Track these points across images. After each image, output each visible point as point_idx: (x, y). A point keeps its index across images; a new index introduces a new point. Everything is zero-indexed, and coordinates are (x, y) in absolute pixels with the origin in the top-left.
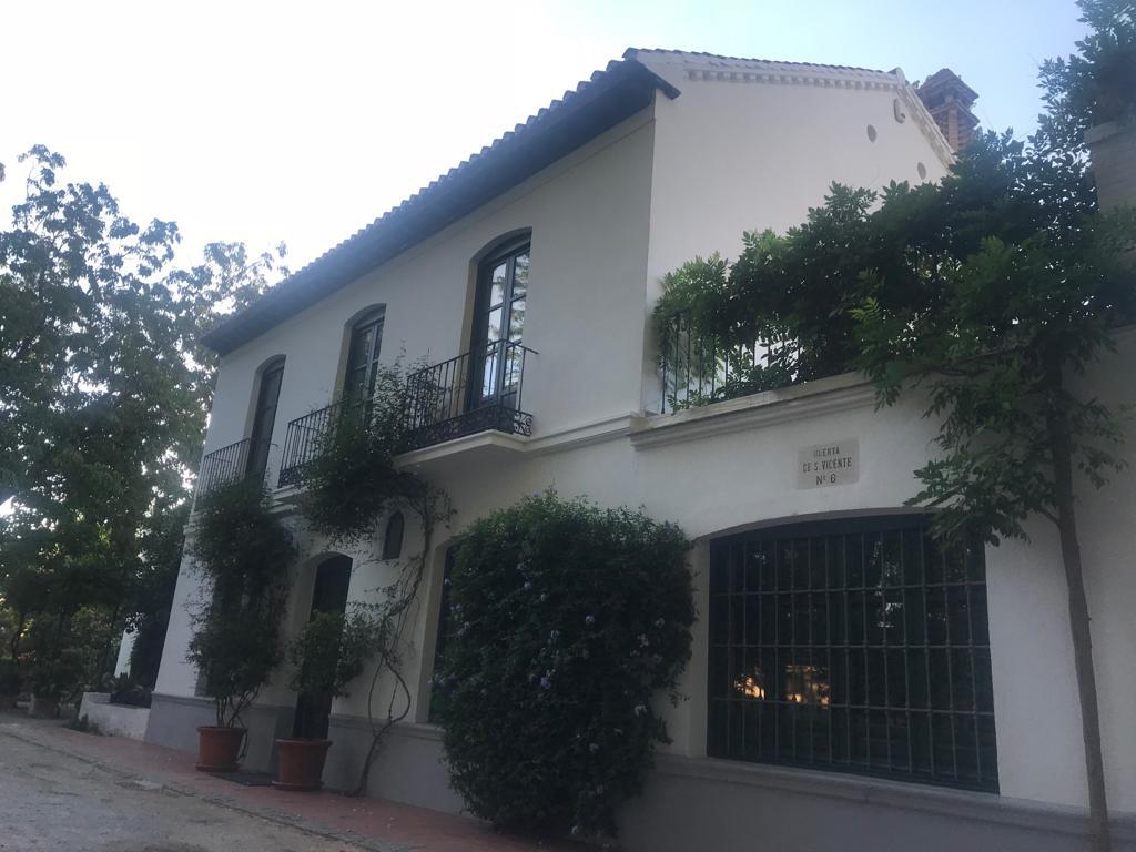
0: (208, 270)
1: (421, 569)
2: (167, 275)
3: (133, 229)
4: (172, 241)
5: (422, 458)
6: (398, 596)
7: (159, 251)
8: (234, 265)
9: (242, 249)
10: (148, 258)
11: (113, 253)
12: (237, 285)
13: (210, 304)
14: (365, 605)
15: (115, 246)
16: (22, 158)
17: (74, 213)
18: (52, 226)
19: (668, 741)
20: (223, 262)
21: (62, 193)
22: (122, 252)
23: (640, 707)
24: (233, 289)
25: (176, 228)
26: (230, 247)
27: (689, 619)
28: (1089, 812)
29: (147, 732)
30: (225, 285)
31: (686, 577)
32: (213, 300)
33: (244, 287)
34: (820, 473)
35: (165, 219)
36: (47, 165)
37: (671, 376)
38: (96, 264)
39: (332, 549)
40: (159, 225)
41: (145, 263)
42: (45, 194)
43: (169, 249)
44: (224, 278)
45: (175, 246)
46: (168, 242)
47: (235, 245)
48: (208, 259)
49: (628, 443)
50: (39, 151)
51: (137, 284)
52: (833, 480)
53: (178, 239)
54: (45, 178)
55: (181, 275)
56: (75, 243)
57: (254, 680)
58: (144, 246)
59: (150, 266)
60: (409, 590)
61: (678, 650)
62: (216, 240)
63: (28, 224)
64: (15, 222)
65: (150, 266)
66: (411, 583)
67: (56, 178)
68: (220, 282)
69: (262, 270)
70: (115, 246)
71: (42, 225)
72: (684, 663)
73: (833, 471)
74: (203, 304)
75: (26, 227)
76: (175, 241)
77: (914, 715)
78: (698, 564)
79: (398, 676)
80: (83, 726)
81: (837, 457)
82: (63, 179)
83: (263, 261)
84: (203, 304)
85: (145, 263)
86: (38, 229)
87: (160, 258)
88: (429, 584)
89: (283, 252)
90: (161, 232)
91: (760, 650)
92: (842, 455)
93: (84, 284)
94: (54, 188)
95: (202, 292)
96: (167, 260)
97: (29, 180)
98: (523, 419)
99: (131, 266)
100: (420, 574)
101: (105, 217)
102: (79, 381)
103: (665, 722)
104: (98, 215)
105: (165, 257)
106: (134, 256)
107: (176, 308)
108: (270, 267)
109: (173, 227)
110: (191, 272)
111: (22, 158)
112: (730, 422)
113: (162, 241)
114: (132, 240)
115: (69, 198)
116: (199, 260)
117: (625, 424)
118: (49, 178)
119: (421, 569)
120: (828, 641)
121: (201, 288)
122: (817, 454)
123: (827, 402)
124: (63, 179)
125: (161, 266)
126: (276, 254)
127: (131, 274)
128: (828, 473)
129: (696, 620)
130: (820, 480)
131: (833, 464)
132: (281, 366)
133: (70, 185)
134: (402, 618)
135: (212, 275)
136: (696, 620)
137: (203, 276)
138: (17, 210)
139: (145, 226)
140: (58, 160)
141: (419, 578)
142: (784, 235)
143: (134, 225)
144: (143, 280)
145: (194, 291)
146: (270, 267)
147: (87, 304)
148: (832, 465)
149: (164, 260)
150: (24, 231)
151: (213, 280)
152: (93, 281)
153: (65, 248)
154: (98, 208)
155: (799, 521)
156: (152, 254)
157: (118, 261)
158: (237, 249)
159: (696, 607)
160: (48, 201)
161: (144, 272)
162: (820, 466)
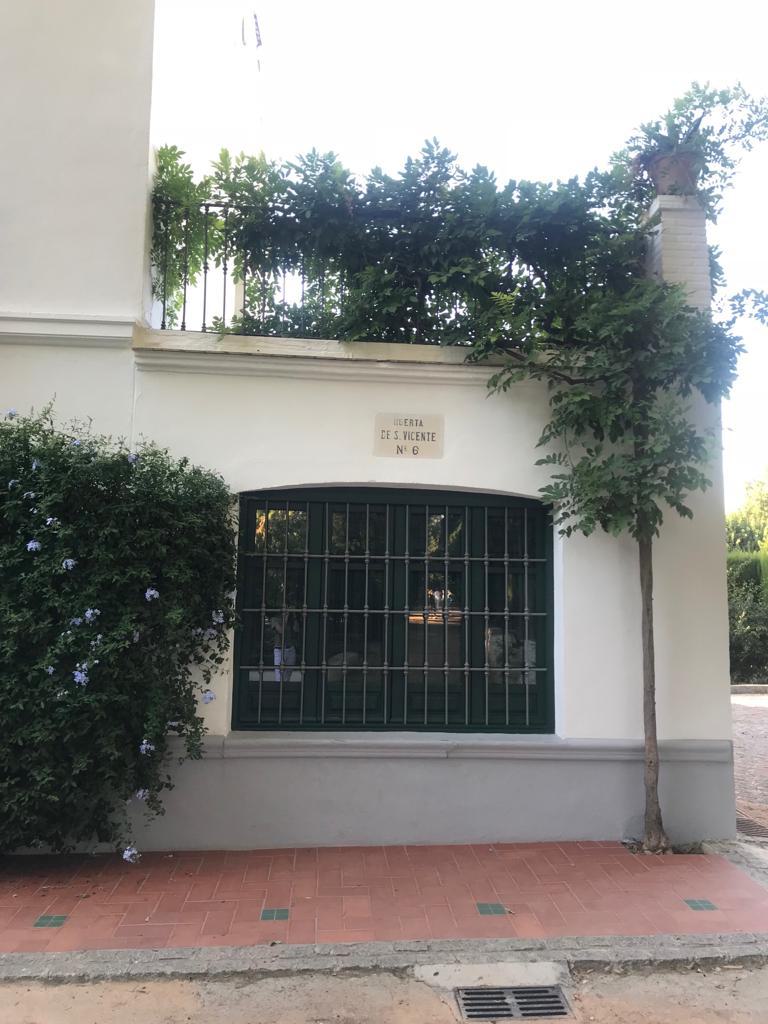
23: (153, 592)
28: (250, 679)
32: (749, 293)
34: (401, 442)
49: (131, 357)
52: (415, 452)
73: (415, 443)
91: (306, 560)
112: (315, 367)
117: (127, 332)
120: (407, 553)
122: (398, 422)
123: (418, 371)
128: (409, 444)
130: (400, 450)
131: (417, 436)
148: (414, 436)
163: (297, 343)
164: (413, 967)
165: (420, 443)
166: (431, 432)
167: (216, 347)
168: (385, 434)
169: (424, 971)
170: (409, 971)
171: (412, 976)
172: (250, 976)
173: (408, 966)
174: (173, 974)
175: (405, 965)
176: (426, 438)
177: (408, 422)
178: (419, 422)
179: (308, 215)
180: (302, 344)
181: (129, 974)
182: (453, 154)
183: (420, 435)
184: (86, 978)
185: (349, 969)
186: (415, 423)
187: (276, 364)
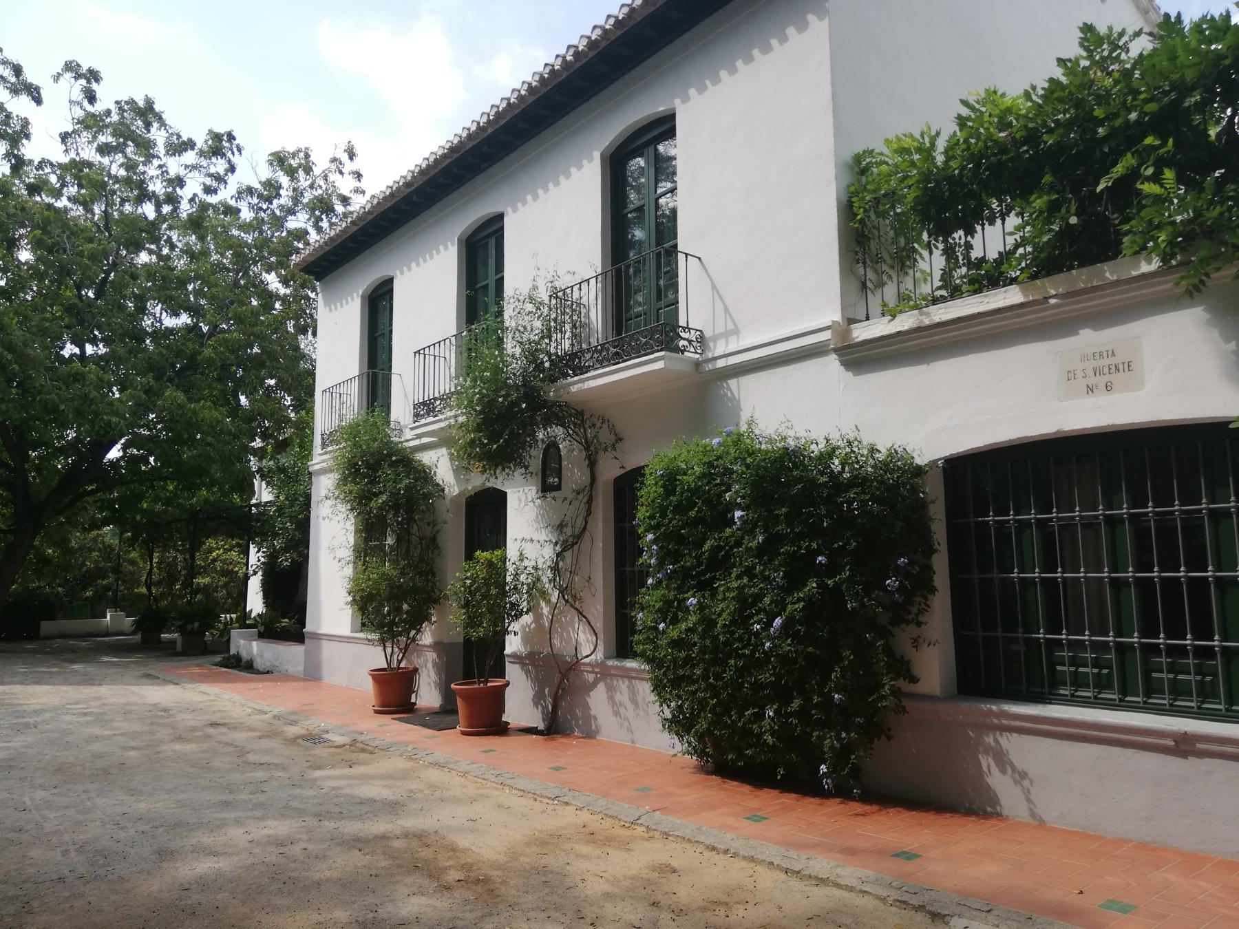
0: (277, 182)
1: (590, 502)
2: (234, 192)
3: (189, 145)
4: (233, 153)
7: (219, 166)
8: (301, 173)
9: (307, 156)
10: (210, 175)
11: (173, 172)
12: (307, 197)
13: (284, 219)
14: (532, 540)
15: (175, 166)
16: (57, 78)
17: (124, 133)
19: (914, 680)
20: (291, 173)
22: (182, 172)
24: (305, 201)
26: (294, 155)
27: (930, 550)
29: (305, 668)
30: (297, 195)
31: (923, 505)
33: (316, 197)
34: (1091, 380)
35: (221, 129)
36: (83, 82)
37: (870, 274)
38: (157, 187)
39: (489, 485)
40: (217, 137)
41: (208, 181)
42: (89, 115)
43: (229, 161)
44: (295, 190)
45: (236, 159)
46: (229, 154)
47: (299, 151)
48: (274, 171)
49: (832, 363)
51: (204, 207)
52: (1108, 388)
53: (239, 150)
54: (86, 97)
55: (250, 191)
56: (130, 166)
57: (417, 620)
58: (204, 163)
59: (214, 184)
60: (580, 523)
62: (278, 149)
63: (80, 151)
64: (66, 151)
65: (214, 184)
68: (291, 193)
69: (333, 177)
70: (175, 166)
71: (94, 151)
73: (1107, 378)
74: (278, 222)
76: (236, 153)
78: (934, 490)
79: (580, 613)
80: (243, 666)
81: (1112, 361)
82: (107, 97)
83: (333, 167)
84: (278, 222)
85: (208, 181)
86: (89, 153)
87: (222, 173)
88: (601, 517)
89: (352, 155)
90: (220, 145)
92: (1118, 360)
93: (149, 210)
94: (98, 108)
95: (272, 207)
96: (229, 174)
97: (71, 102)
99: (193, 186)
100: (590, 507)
101: (158, 136)
102: (161, 314)
103: (909, 662)
104: (149, 131)
105: (227, 171)
106: (195, 173)
107: (246, 227)
108: (341, 173)
109: (231, 137)
110: (258, 186)
111: (57, 78)
113: (223, 155)
114: (190, 157)
115: (115, 118)
116: (265, 173)
118: (91, 97)
119: (590, 502)
121: (271, 204)
122: (1084, 358)
125: (226, 183)
126: (344, 157)
127: (195, 195)
128: (1101, 380)
130: (1090, 389)
132: (388, 288)
133: (117, 102)
135: (280, 187)
136: (936, 551)
137: (272, 188)
138: (65, 137)
139: (201, 140)
140: (93, 76)
141: (589, 512)
143: (190, 140)
144: (212, 199)
145: (265, 207)
146: (341, 173)
148: (1106, 370)
149: (226, 175)
150: (78, 159)
151: (283, 192)
153: (122, 172)
154: (148, 125)
155: (1061, 436)
156: (212, 170)
157: (179, 182)
158: (301, 155)
160: (92, 123)
161: (208, 190)
162: (1090, 372)
164: (952, 916)
165: (1115, 377)
166: (1126, 361)
168: (1071, 375)
170: (947, 918)
173: (948, 915)
176: (1121, 369)
178: (1110, 353)
179: (481, 124)
180: (980, 300)
181: (753, 857)
184: (1026, 783)
186: (1105, 354)
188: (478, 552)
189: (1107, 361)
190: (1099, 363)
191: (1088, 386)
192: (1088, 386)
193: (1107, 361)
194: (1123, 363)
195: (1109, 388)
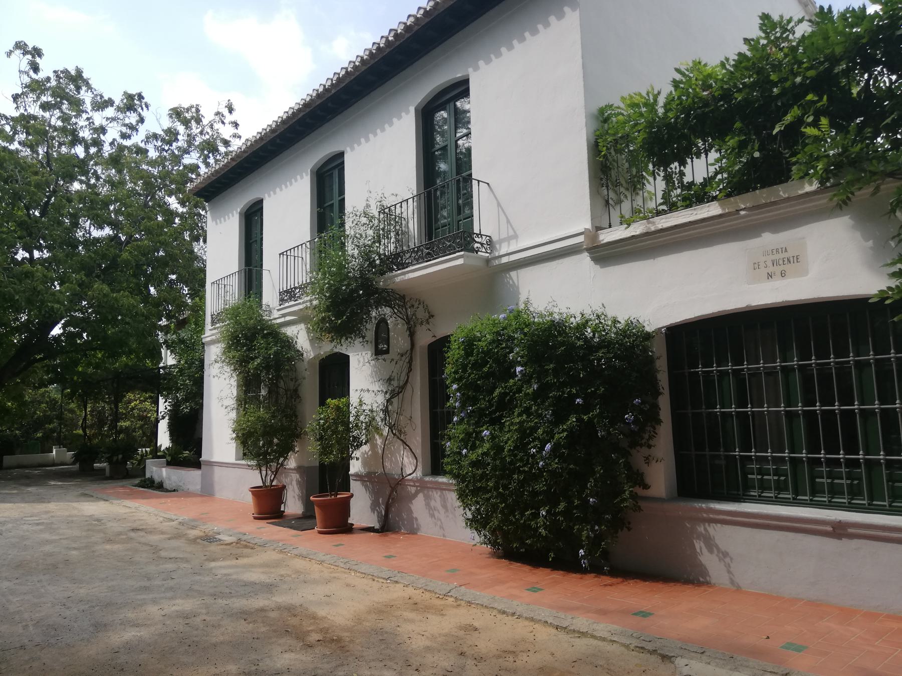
0: (175, 130)
1: (410, 362)
2: (143, 137)
3: (110, 102)
5: (398, 279)
6: (395, 383)
7: (132, 118)
9: (198, 111)
12: (198, 140)
15: (99, 118)
16: (9, 54)
18: (45, 107)
19: (646, 487)
20: (186, 123)
21: (48, 79)
22: (104, 123)
24: (197, 143)
25: (143, 98)
26: (188, 110)
27: (657, 393)
30: (191, 139)
31: (651, 361)
33: (204, 141)
34: (771, 269)
36: (29, 57)
37: (612, 195)
38: (86, 134)
40: (130, 97)
41: (124, 129)
43: (140, 115)
44: (189, 135)
45: (145, 113)
46: (139, 110)
47: (192, 107)
49: (585, 259)
50: (20, 46)
51: (121, 148)
52: (783, 275)
53: (147, 106)
55: (155, 136)
56: (65, 118)
57: (285, 450)
58: (121, 116)
59: (129, 131)
61: (651, 417)
63: (27, 108)
64: (17, 108)
65: (129, 131)
66: (404, 374)
67: (40, 67)
68: (186, 138)
70: (99, 118)
71: (38, 107)
72: (655, 428)
73: (782, 268)
74: (177, 159)
75: (26, 110)
77: (867, 461)
78: (659, 350)
80: (158, 486)
81: (786, 255)
82: (47, 69)
83: (217, 118)
84: (177, 159)
85: (124, 129)
86: (34, 109)
87: (134, 123)
90: (132, 102)
93: (80, 151)
94: (41, 76)
95: (172, 148)
96: (140, 124)
97: (20, 72)
98: (484, 240)
99: (113, 133)
100: (411, 365)
101: (86, 97)
102: (90, 227)
104: (79, 93)
105: (138, 122)
106: (114, 124)
107: (152, 163)
108: (223, 123)
109: (141, 97)
110: (162, 133)
111: (9, 54)
113: (135, 110)
114: (110, 112)
116: (167, 123)
118: (36, 68)
122: (766, 253)
124: (47, 69)
125: (137, 130)
126: (225, 112)
127: (114, 140)
128: (777, 269)
129: (661, 394)
130: (770, 276)
134: (400, 400)
135: (178, 134)
136: (661, 394)
137: (172, 135)
138: (16, 98)
139: (118, 100)
141: (410, 370)
142: (350, 521)
143: (110, 99)
145: (166, 148)
146: (223, 123)
147: (82, 166)
148: (781, 262)
149: (137, 125)
151: (180, 137)
152: (87, 149)
153: (59, 123)
154: (78, 89)
156: (127, 121)
157: (102, 130)
158: (194, 110)
159: (660, 383)
160: (36, 87)
161: (124, 136)
162: (769, 264)
163: (686, 213)
165: (787, 267)
167: (636, 232)
168: (756, 266)
169: (680, 662)
171: (673, 662)
172: (31, 517)
173: (674, 656)
174: (551, 623)
175: (672, 655)
176: (792, 261)
177: (775, 252)
178: (784, 250)
180: (690, 212)
182: (826, 7)
183: (786, 260)
185: (639, 647)
187: (769, 212)
188: (329, 400)
189: (781, 256)
190: (776, 257)
191: (768, 273)
192: (768, 273)
193: (781, 256)
194: (793, 257)
195: (783, 275)
